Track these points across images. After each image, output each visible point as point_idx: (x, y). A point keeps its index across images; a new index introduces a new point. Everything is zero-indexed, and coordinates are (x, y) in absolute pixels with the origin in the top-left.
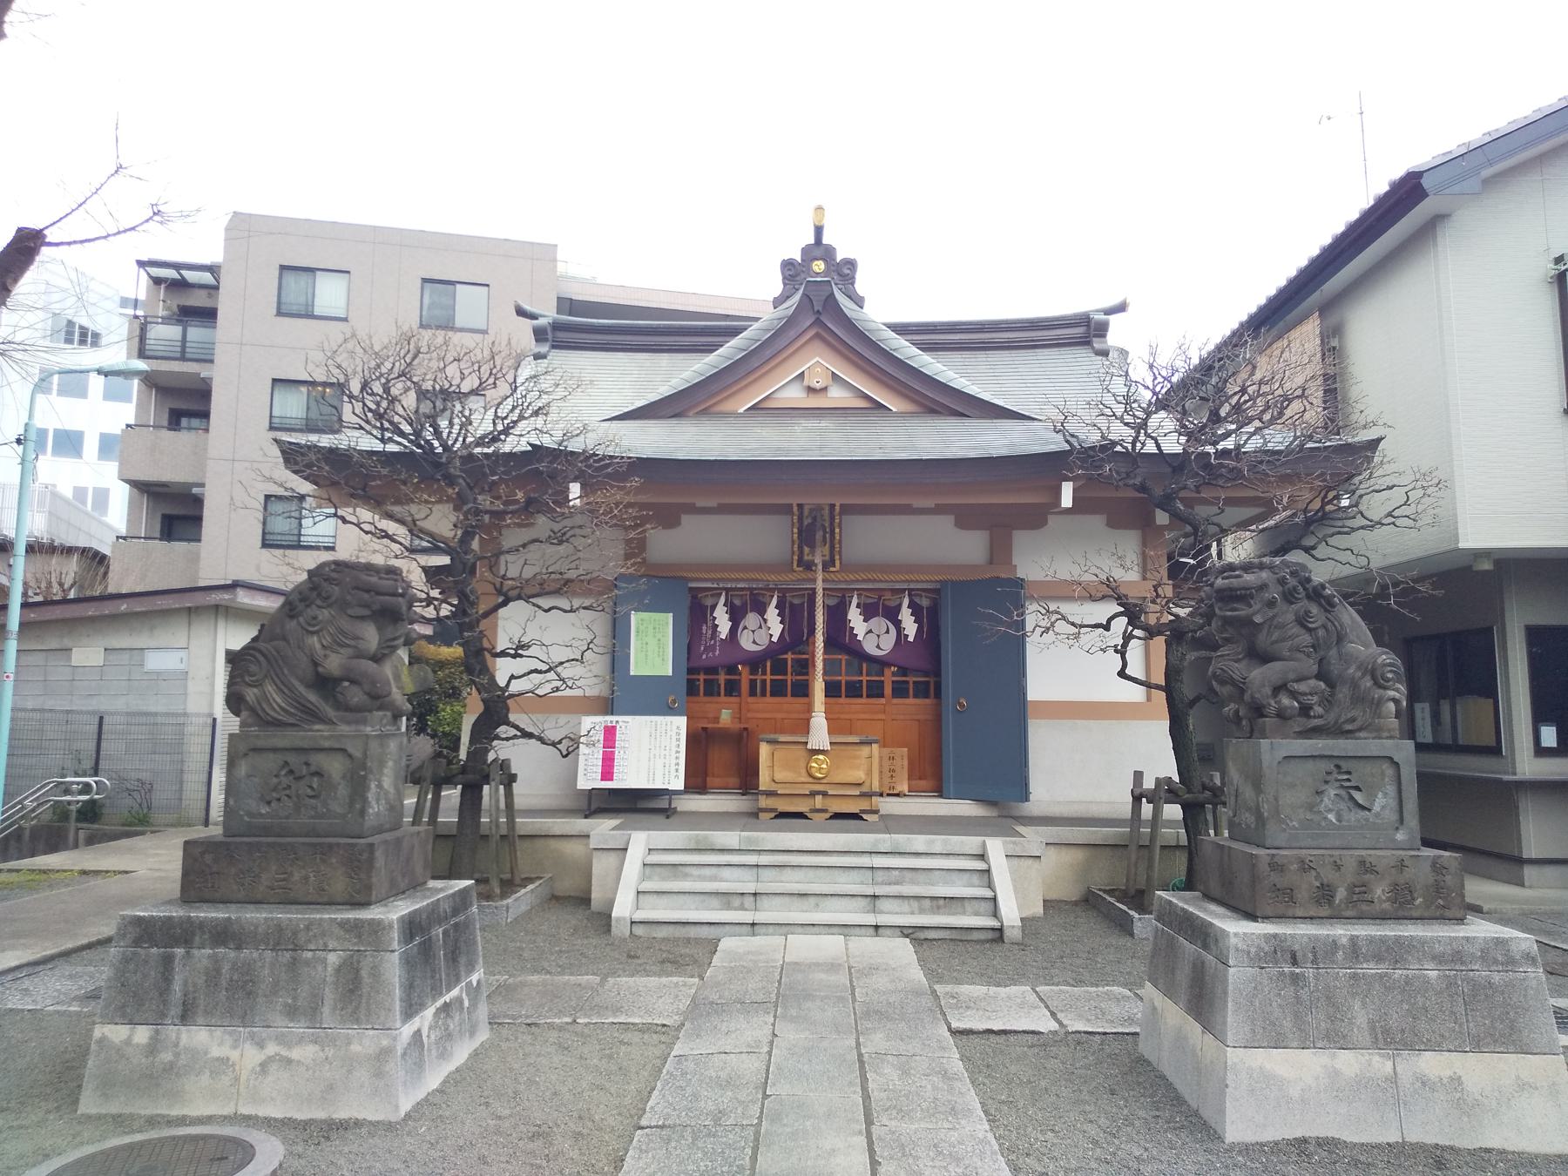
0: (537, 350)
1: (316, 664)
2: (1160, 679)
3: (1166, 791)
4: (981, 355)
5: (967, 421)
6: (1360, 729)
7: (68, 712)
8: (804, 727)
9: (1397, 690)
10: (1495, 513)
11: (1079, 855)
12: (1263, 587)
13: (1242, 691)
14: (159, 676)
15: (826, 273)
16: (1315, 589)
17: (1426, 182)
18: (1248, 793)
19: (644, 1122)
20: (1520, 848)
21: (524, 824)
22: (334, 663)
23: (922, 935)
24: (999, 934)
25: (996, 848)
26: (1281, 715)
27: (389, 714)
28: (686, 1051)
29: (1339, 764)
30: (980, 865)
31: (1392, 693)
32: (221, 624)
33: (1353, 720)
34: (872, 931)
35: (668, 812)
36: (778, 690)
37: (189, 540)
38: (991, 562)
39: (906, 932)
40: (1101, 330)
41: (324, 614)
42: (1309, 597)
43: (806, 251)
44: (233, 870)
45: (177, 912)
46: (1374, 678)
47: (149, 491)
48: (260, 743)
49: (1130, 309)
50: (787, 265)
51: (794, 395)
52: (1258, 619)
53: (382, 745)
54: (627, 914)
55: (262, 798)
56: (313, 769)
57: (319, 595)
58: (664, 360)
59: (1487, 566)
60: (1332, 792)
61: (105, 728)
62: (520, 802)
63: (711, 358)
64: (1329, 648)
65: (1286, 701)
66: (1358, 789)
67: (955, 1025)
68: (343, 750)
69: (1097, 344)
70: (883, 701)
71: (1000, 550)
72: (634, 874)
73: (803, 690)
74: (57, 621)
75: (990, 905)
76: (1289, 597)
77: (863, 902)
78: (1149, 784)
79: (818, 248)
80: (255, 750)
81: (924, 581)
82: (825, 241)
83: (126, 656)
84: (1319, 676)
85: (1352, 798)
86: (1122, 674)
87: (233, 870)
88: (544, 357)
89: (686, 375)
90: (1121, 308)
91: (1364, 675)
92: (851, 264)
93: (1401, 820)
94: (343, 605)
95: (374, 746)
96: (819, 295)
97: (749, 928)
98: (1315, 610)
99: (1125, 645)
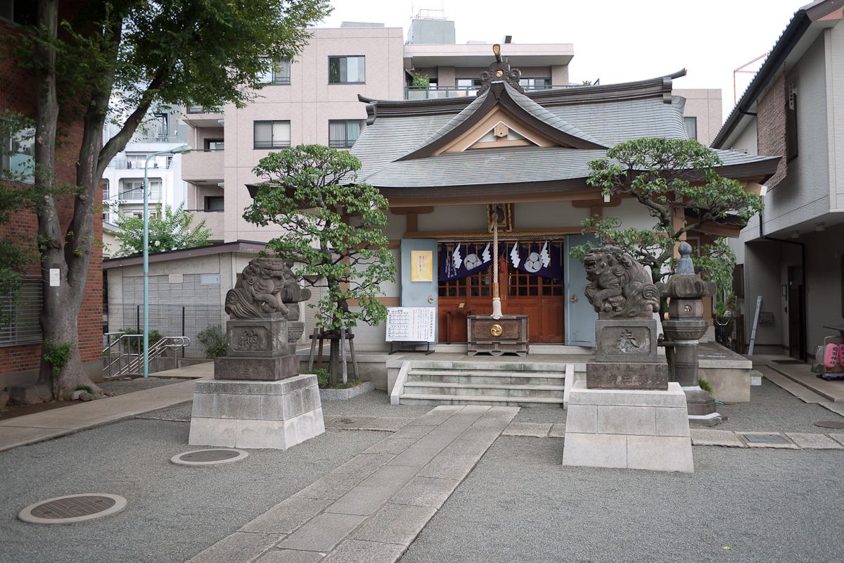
1: (253, 296)
6: (636, 316)
7: (169, 305)
12: (600, 260)
14: (208, 287)
15: (502, 78)
17: (810, 16)
21: (359, 357)
22: (259, 296)
23: (527, 405)
29: (628, 329)
30: (561, 376)
31: (649, 301)
32: (234, 260)
33: (633, 312)
34: (505, 404)
35: (428, 352)
37: (218, 211)
40: (668, 88)
41: (254, 278)
44: (230, 368)
46: (642, 295)
47: (199, 185)
48: (237, 325)
51: (489, 142)
52: (598, 273)
61: (185, 312)
62: (356, 348)
63: (457, 116)
69: (666, 97)
72: (403, 376)
74: (161, 262)
76: (610, 263)
77: (503, 392)
81: (556, 236)
83: (192, 278)
84: (623, 294)
87: (230, 368)
89: (445, 126)
90: (682, 73)
91: (638, 295)
94: (261, 275)
95: (274, 326)
98: (620, 268)
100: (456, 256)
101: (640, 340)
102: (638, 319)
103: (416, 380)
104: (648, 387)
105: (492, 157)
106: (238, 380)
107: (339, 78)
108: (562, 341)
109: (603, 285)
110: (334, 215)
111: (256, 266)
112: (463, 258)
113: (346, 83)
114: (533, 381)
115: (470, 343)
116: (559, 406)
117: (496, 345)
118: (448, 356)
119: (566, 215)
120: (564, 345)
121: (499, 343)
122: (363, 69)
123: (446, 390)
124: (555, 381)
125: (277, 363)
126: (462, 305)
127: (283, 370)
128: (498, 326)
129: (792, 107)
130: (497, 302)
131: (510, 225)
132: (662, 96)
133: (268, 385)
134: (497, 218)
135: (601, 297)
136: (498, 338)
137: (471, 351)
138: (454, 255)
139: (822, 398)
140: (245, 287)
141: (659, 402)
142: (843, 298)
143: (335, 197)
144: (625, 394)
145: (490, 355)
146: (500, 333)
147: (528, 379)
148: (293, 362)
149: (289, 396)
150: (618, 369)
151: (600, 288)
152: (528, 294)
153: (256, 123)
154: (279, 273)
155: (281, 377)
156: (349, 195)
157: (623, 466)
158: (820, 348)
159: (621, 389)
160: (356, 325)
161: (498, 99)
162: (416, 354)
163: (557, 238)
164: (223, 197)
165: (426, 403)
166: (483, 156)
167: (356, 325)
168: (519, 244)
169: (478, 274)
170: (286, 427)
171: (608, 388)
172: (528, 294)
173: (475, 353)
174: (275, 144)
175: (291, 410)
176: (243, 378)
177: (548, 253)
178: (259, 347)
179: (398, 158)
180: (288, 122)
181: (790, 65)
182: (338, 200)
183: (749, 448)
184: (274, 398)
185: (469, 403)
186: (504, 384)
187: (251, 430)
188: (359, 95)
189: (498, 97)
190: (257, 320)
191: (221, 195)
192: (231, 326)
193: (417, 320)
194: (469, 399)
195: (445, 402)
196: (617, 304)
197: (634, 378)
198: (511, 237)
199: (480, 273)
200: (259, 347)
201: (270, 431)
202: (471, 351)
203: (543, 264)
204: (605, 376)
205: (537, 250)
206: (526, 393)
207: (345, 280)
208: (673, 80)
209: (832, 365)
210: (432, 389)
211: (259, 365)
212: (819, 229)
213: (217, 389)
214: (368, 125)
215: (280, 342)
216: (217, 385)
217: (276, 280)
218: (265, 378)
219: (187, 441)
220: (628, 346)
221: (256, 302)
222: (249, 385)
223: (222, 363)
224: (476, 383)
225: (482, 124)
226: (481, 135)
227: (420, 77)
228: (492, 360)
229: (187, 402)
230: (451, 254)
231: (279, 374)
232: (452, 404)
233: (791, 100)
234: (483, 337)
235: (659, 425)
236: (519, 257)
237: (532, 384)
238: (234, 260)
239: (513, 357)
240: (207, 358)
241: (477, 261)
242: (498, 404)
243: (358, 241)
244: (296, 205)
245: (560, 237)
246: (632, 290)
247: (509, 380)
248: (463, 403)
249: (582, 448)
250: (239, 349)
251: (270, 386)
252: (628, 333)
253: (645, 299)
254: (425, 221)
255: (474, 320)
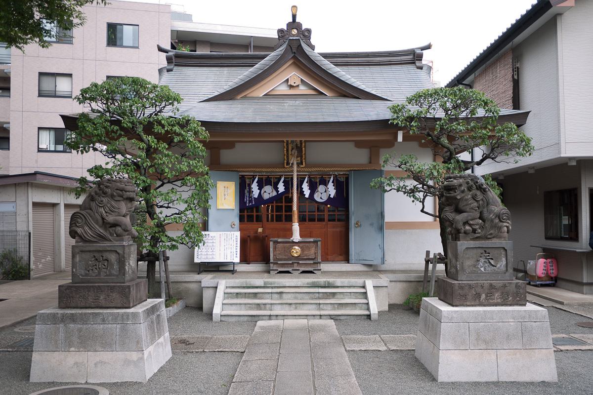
0: (168, 67)
1: (103, 219)
2: (438, 214)
3: (441, 259)
4: (367, 68)
5: (360, 101)
6: (494, 237)
8: (290, 233)
9: (508, 223)
10: (575, 145)
11: (404, 285)
12: (460, 185)
13: (453, 224)
16: (479, 185)
18: (454, 261)
19: (234, 381)
20: (422, 271)
21: (173, 278)
22: (111, 219)
23: (338, 318)
24: (369, 317)
25: (370, 284)
26: (465, 233)
27: (130, 236)
28: (247, 359)
29: (486, 250)
30: (363, 290)
31: (505, 224)
32: (30, 191)
33: (491, 234)
34: (318, 317)
35: (233, 272)
36: (279, 219)
38: (370, 163)
39: (331, 317)
40: (420, 57)
41: (105, 200)
42: (477, 189)
43: (289, 25)
44: (78, 296)
45: (71, 285)
48: (84, 249)
49: (432, 47)
50: (280, 31)
51: (284, 90)
52: (459, 197)
53: (129, 249)
54: (219, 312)
55: (86, 269)
56: (104, 258)
57: (103, 192)
58: (226, 70)
59: (574, 163)
60: (482, 260)
62: (170, 268)
63: (251, 69)
64: (484, 208)
65: (468, 228)
66: (492, 259)
67: (348, 349)
68: (116, 251)
70: (324, 223)
71: (374, 157)
72: (221, 296)
73: (289, 219)
75: (366, 306)
77: (314, 306)
78: (431, 256)
79: (294, 24)
80: (82, 251)
81: (340, 171)
82: (297, 20)
84: (480, 218)
85: (490, 262)
86: (422, 211)
87: (78, 296)
88: (171, 70)
90: (429, 47)
91: (495, 217)
92: (309, 31)
93: (507, 270)
94: (112, 196)
95: (127, 250)
96: (294, 45)
97: (267, 317)
98: (478, 193)
99: (424, 199)
100: (255, 187)
101: (497, 260)
102: (495, 241)
103: (232, 298)
104: (509, 303)
105: (284, 100)
106: (86, 308)
107: (116, 42)
108: (347, 260)
109: (463, 208)
110: (161, 144)
111: (107, 187)
112: (260, 188)
113: (122, 46)
114: (338, 296)
115: (272, 263)
116: (366, 317)
117: (296, 264)
118: (254, 276)
119: (352, 155)
120: (348, 263)
121: (298, 263)
122: (136, 36)
123: (262, 306)
124: (357, 295)
125: (131, 289)
126: (260, 230)
127: (136, 297)
128: (297, 247)
129: (516, 77)
130: (296, 227)
131: (304, 161)
132: (414, 63)
133: (125, 313)
134: (296, 154)
135: (462, 220)
136: (298, 258)
137: (273, 270)
138: (252, 187)
139: (548, 301)
140: (94, 208)
141: (524, 317)
142: (568, 224)
143: (163, 126)
144: (494, 311)
145: (290, 273)
146: (299, 254)
147: (334, 294)
148: (143, 287)
149: (146, 324)
150: (482, 287)
151: (459, 211)
152: (246, 220)
153: (41, 74)
154: (132, 195)
155: (135, 304)
156: (175, 126)
157: (494, 379)
158: (532, 262)
159: (485, 306)
160: (178, 249)
161: (294, 53)
162: (219, 273)
163: (342, 173)
164: (8, 138)
165: (246, 318)
166: (281, 101)
167: (178, 249)
168: (309, 177)
169: (273, 203)
170: (145, 356)
171: (472, 306)
172: (246, 220)
173: (277, 272)
174: (58, 93)
175: (148, 337)
176: (93, 306)
177: (334, 186)
178: (110, 271)
179: (204, 99)
180: (70, 75)
181: (515, 47)
182: (166, 129)
183: (561, 351)
184: (132, 326)
185: (286, 317)
186: (312, 299)
187: (105, 363)
188: (158, 45)
189: (294, 51)
190: (108, 244)
191: (7, 136)
192: (77, 250)
193: (223, 244)
194: (286, 314)
195: (264, 318)
196: (477, 227)
197: (496, 295)
198: (303, 171)
199: (275, 202)
200: (110, 271)
201: (127, 362)
202: (273, 270)
203: (330, 195)
204: (470, 294)
205: (325, 183)
206: (334, 307)
207: (166, 205)
208: (424, 51)
209: (543, 275)
210: (249, 305)
211: (112, 292)
212: (531, 171)
213: (63, 319)
214: (168, 71)
215: (131, 266)
216: (63, 315)
217: (128, 202)
218: (119, 305)
219: (28, 377)
220: (486, 265)
221: (105, 224)
222: (101, 313)
223: (68, 291)
224: (287, 299)
225: (278, 75)
226: (276, 84)
227: (182, 48)
228: (291, 278)
229: (3, 327)
230: (250, 185)
231: (133, 300)
232: (270, 319)
233: (515, 71)
234: (284, 257)
235: (525, 339)
236: (309, 189)
237: (338, 298)
238: (30, 191)
239: (310, 274)
240: (2, 279)
241: (272, 192)
242: (312, 317)
243: (185, 168)
244: (123, 133)
245: (344, 172)
246: (490, 213)
247: (317, 295)
248: (280, 317)
249: (455, 364)
250: (86, 275)
251: (128, 314)
252: (485, 253)
253: (502, 222)
254: (227, 156)
255: (276, 242)
